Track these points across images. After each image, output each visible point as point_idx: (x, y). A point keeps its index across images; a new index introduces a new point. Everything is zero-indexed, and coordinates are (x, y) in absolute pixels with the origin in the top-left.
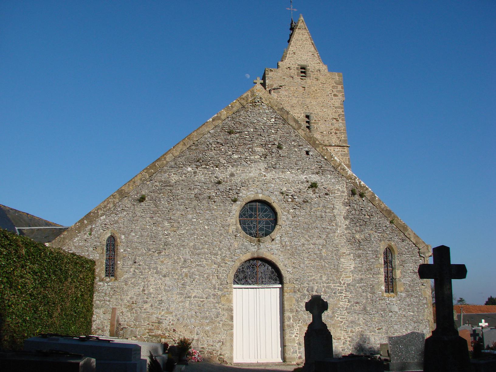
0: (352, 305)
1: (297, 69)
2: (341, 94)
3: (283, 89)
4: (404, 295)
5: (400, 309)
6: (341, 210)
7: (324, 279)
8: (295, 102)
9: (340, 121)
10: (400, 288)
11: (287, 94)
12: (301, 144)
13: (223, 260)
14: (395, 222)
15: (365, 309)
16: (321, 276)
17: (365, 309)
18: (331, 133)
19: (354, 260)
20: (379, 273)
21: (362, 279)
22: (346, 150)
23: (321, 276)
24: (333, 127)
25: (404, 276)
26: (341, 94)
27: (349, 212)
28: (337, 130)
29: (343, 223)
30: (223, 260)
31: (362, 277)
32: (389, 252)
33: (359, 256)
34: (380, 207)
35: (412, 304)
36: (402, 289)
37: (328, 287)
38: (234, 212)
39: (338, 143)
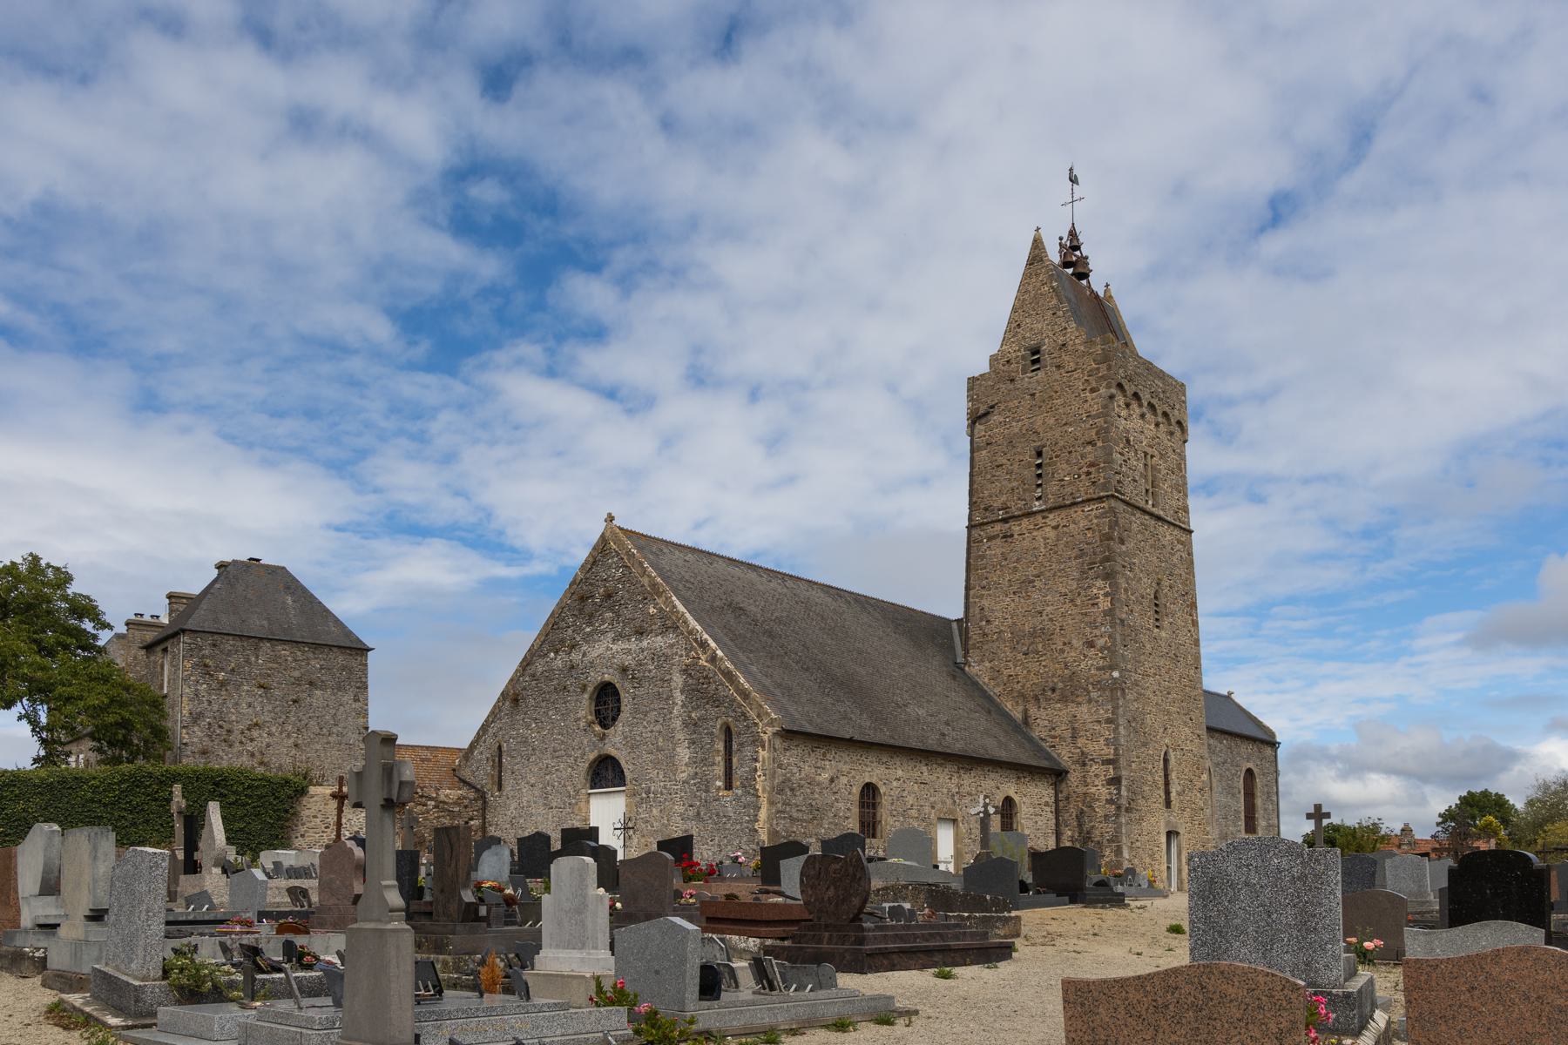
1: (1023, 357)
10: (736, 783)
27: (685, 681)
28: (1092, 465)
29: (679, 698)
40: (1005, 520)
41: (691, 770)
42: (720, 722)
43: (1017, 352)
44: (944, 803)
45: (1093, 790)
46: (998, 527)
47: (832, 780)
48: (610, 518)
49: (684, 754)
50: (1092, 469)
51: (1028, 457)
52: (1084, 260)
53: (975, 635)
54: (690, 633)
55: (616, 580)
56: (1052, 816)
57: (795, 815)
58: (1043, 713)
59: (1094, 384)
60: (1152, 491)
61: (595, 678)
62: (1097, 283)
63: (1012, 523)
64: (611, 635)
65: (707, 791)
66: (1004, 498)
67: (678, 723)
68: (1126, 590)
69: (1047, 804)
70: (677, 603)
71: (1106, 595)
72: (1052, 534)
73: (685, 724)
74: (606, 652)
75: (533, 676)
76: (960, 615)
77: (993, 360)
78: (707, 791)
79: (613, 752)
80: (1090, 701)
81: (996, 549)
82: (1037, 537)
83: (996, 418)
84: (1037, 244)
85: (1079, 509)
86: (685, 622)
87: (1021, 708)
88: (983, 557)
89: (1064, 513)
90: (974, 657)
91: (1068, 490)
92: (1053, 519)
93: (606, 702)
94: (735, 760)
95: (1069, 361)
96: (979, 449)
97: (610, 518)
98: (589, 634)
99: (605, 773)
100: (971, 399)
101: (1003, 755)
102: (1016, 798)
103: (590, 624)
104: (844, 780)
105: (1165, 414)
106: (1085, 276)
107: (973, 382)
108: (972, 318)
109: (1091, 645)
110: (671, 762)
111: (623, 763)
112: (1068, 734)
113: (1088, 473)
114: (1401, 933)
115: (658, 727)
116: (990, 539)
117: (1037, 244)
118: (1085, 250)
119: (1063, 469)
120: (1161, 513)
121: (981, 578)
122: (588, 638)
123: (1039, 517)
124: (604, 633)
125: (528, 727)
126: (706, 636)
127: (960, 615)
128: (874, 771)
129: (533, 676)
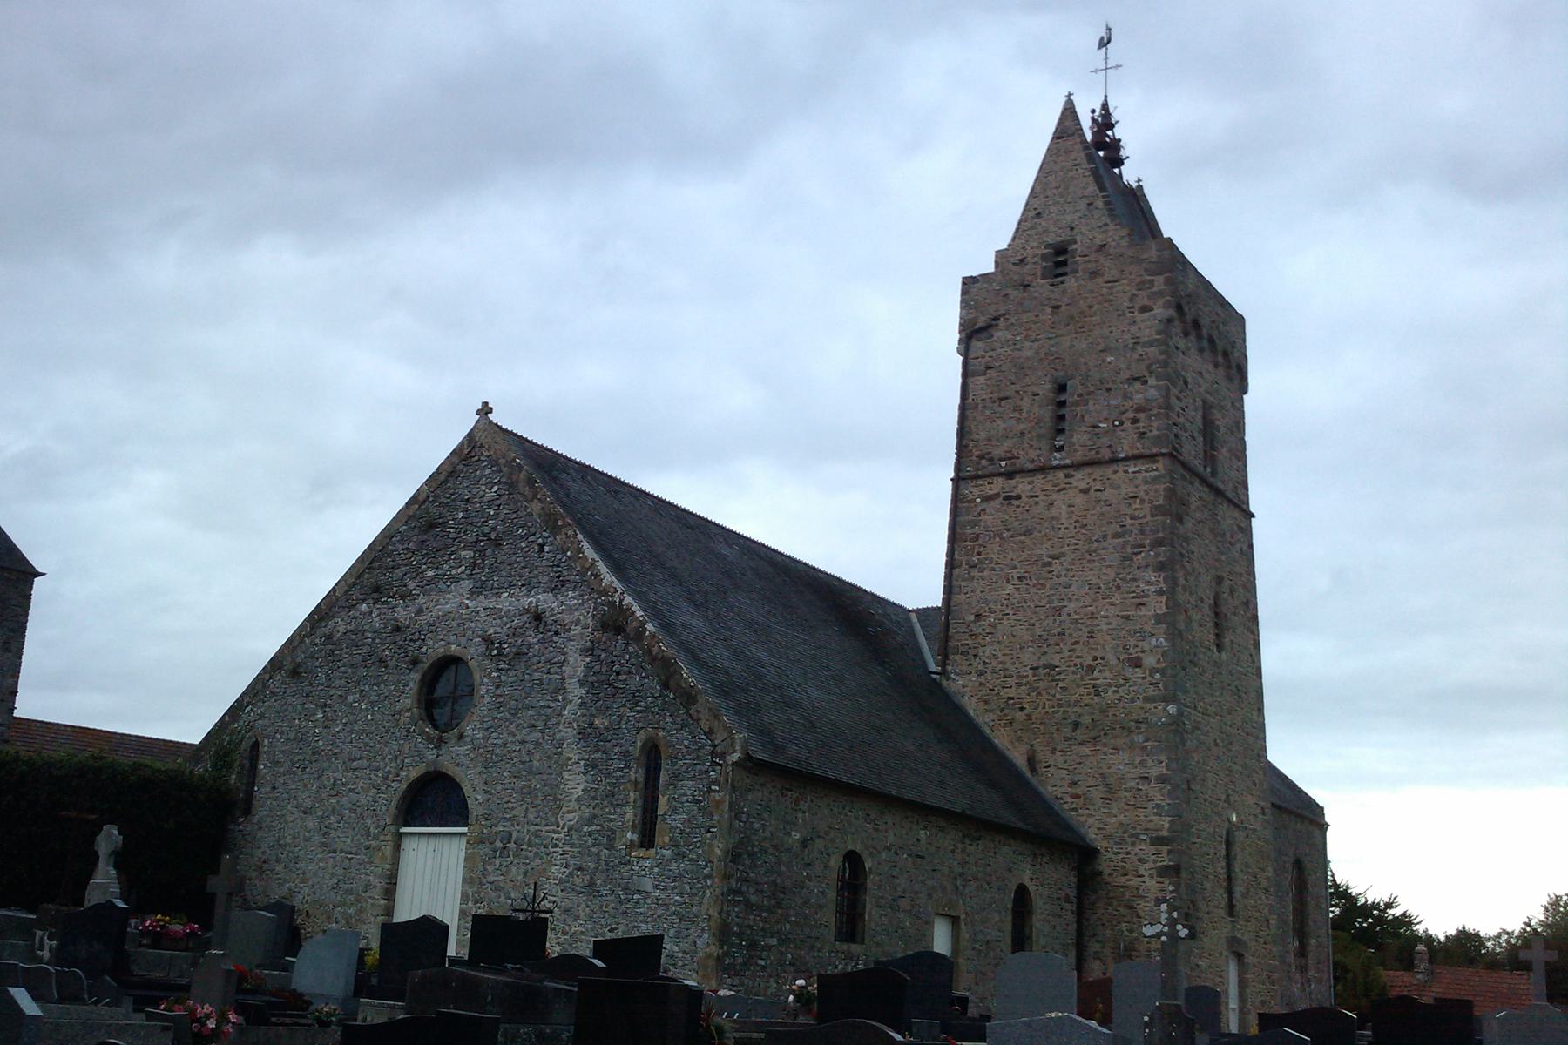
0: (571, 874)
1: (1044, 257)
2: (1161, 302)
3: (1001, 322)
4: (667, 853)
5: (656, 887)
6: (576, 664)
7: (531, 817)
8: (1029, 353)
9: (1152, 381)
10: (662, 838)
11: (1009, 337)
12: (532, 530)
13: (386, 778)
14: (672, 683)
15: (592, 884)
16: (526, 811)
17: (592, 884)
18: (1121, 423)
19: (585, 774)
20: (626, 804)
21: (595, 816)
22: (1160, 466)
23: (526, 811)
24: (1129, 404)
25: (674, 810)
26: (1161, 302)
27: (588, 667)
28: (1140, 409)
29: (576, 692)
30: (386, 778)
31: (596, 811)
32: (652, 756)
33: (594, 767)
34: (650, 652)
35: (681, 876)
36: (667, 839)
37: (536, 834)
38: (411, 684)
39: (1140, 448)
40: (1009, 475)
41: (587, 812)
42: (642, 735)
43: (1035, 250)
44: (944, 889)
45: (1135, 882)
46: (998, 484)
47: (804, 844)
48: (486, 410)
49: (575, 783)
50: (1142, 416)
51: (1045, 389)
52: (1115, 145)
53: (959, 637)
54: (604, 592)
55: (506, 503)
56: (1072, 918)
57: (753, 899)
58: (1059, 758)
59: (1146, 302)
60: (1210, 458)
61: (435, 648)
62: (1129, 173)
63: (1018, 479)
64: (467, 585)
65: (610, 847)
66: (1007, 444)
67: (568, 733)
68: (1184, 589)
69: (1067, 899)
70: (585, 544)
71: (1160, 593)
72: (1080, 500)
73: (583, 735)
74: (456, 611)
75: (329, 637)
76: (935, 599)
77: (1001, 256)
78: (610, 847)
79: (450, 769)
80: (1132, 746)
81: (993, 516)
82: (1063, 502)
83: (999, 334)
84: (1069, 111)
85: (1121, 467)
86: (596, 576)
87: (1023, 748)
88: (975, 524)
89: (1098, 471)
90: (957, 663)
91: (1106, 440)
92: (1080, 479)
93: (442, 690)
94: (663, 802)
95: (1110, 269)
96: (975, 374)
97: (486, 410)
98: (433, 581)
99: (433, 800)
100: (965, 304)
101: (934, 798)
102: (1032, 888)
103: (434, 565)
104: (819, 844)
105: (1225, 354)
106: (1119, 162)
107: (969, 283)
108: (979, 202)
109: (1136, 663)
110: (554, 801)
111: (467, 788)
112: (1096, 794)
113: (1135, 421)
114: (931, 925)
115: (536, 735)
116: (987, 499)
117: (1069, 111)
118: (1118, 132)
119: (1097, 409)
120: (1220, 485)
121: (969, 552)
122: (428, 587)
123: (1060, 474)
124: (455, 580)
125: (308, 716)
126: (628, 600)
127: (935, 599)
128: (859, 830)
129: (329, 637)
